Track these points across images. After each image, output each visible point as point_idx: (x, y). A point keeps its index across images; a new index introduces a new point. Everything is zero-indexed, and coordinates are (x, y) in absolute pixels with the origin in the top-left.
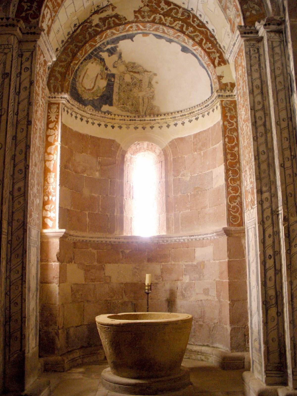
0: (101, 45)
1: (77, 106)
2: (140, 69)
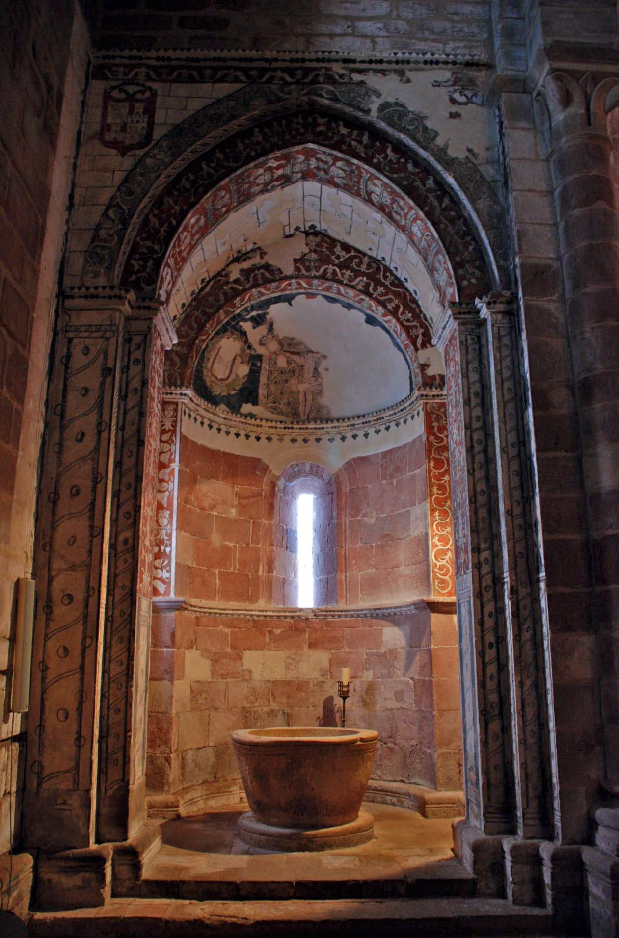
0: (241, 311)
1: (203, 407)
2: (301, 348)
